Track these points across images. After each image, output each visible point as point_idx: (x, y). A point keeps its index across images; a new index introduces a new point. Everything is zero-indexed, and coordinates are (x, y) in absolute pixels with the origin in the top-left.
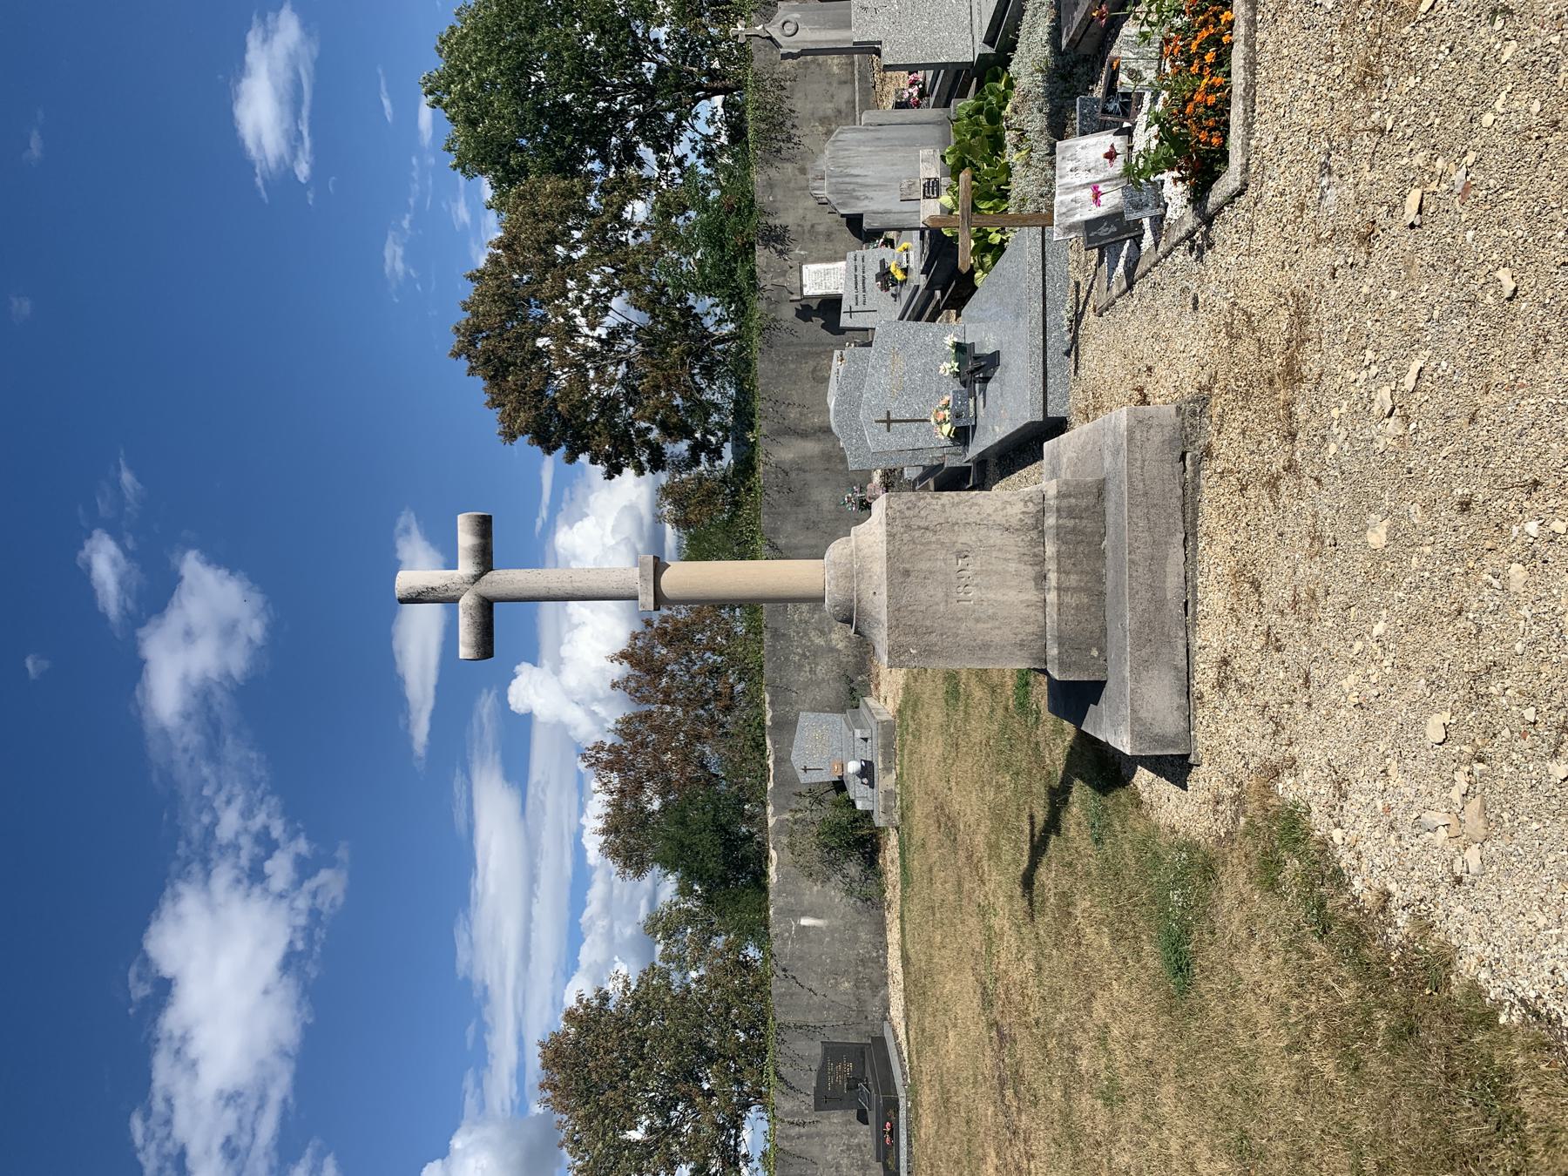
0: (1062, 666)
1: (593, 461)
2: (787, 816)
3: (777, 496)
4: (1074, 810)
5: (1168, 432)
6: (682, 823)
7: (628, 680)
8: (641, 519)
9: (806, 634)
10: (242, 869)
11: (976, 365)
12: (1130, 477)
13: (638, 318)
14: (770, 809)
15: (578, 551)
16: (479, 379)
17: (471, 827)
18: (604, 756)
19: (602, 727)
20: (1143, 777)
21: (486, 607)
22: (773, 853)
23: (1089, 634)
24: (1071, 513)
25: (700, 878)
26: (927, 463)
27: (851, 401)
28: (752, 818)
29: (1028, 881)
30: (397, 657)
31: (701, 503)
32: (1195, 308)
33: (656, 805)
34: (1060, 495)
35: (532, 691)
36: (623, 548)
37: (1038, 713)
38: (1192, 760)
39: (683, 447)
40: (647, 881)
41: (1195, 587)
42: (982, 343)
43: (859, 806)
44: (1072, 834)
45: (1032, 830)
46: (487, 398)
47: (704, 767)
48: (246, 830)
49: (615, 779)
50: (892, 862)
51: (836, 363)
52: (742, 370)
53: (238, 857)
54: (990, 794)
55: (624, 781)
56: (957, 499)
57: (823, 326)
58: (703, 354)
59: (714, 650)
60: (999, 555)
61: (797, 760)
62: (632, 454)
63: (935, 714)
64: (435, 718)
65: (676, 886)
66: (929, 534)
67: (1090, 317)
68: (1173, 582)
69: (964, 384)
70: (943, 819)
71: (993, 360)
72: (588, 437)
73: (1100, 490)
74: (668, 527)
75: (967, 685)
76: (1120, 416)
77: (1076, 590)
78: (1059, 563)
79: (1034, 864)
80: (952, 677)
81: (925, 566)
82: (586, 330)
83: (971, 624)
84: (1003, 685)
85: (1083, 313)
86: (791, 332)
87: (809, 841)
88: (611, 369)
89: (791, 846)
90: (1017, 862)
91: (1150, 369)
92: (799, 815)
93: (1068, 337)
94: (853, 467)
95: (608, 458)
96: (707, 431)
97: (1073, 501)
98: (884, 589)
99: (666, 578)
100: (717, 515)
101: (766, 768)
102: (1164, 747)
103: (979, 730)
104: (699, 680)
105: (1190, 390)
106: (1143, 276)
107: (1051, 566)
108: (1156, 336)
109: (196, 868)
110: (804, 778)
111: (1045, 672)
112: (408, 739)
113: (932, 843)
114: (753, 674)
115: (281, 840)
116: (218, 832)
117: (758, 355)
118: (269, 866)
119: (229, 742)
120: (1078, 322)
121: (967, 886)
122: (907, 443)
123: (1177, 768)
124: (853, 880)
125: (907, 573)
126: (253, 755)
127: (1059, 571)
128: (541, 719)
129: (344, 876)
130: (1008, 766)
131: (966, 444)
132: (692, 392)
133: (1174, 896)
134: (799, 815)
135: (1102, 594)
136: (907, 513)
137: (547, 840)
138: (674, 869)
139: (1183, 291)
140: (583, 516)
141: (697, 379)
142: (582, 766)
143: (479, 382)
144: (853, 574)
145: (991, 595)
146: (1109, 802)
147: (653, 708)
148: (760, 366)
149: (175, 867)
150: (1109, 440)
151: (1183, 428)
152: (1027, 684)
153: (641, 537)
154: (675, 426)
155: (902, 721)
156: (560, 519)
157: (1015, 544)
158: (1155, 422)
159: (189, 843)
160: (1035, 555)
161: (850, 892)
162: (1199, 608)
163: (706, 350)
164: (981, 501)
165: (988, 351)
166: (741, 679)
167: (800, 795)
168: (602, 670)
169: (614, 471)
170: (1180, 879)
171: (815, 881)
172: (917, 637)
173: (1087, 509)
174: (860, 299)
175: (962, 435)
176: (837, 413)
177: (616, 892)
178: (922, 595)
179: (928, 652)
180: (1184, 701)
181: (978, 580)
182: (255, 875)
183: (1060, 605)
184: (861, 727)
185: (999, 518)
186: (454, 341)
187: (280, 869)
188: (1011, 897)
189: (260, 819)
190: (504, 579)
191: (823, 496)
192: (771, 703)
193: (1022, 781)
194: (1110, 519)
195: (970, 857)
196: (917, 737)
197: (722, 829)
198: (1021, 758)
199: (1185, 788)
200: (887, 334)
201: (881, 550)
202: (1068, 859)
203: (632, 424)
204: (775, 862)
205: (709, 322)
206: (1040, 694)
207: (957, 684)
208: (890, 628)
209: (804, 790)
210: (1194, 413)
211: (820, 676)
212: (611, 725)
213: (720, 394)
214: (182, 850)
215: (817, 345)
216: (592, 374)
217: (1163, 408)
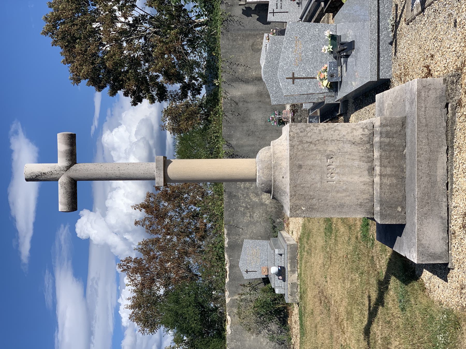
0: (382, 216)
1: (126, 94)
2: (237, 297)
3: (231, 117)
4: (391, 293)
5: (439, 93)
6: (177, 302)
7: (145, 220)
9: (248, 195)
11: (342, 48)
12: (418, 116)
13: (151, 11)
14: (227, 293)
15: (116, 145)
17: (55, 303)
18: (132, 265)
19: (130, 247)
20: (426, 275)
21: (73, 183)
22: (228, 318)
23: (396, 198)
24: (388, 135)
25: (187, 333)
26: (315, 101)
27: (273, 65)
28: (216, 299)
29: (367, 331)
30: (11, 205)
31: (187, 119)
32: (455, 26)
33: (162, 291)
34: (382, 125)
35: (89, 226)
36: (141, 144)
37: (373, 240)
38: (449, 266)
39: (178, 86)
40: (156, 336)
41: (452, 175)
42: (345, 35)
43: (277, 291)
44: (390, 306)
45: (370, 304)
46: (63, 58)
47: (190, 271)
50: (295, 322)
51: (265, 41)
52: (212, 45)
54: (348, 285)
56: (327, 127)
57: (258, 19)
58: (189, 33)
59: (195, 204)
60: (349, 157)
61: (242, 266)
62: (148, 91)
63: (319, 240)
64: (34, 241)
65: (173, 338)
66: (312, 146)
67: (403, 24)
68: (441, 172)
69: (335, 58)
70: (323, 299)
71: (351, 46)
72: (122, 80)
73: (403, 123)
74: (168, 133)
75: (336, 225)
76: (414, 84)
77: (390, 176)
78: (381, 162)
79: (370, 323)
80: (328, 221)
81: (310, 162)
82: (123, 19)
83: (334, 194)
84: (355, 225)
85: (399, 22)
86: (240, 23)
87: (249, 311)
89: (239, 314)
90: (361, 321)
91: (432, 56)
92: (243, 297)
93: (392, 34)
94: (274, 103)
95: (134, 93)
96: (192, 78)
97: (389, 128)
98: (288, 175)
100: (197, 128)
101: (224, 271)
102: (435, 259)
103: (343, 249)
104: (186, 221)
105: (451, 69)
106: (430, 5)
107: (377, 163)
108: (435, 38)
110: (246, 276)
111: (373, 219)
112: (17, 252)
113: (317, 312)
114: (217, 218)
117: (221, 36)
120: (397, 27)
121: (335, 335)
122: (304, 90)
123: (442, 270)
124: (274, 333)
125: (300, 167)
127: (381, 166)
128: (95, 242)
130: (358, 269)
131: (336, 91)
132: (182, 56)
133: (440, 338)
134: (243, 297)
135: (403, 178)
136: (301, 134)
137: (99, 310)
138: (172, 328)
139: (449, 15)
140: (118, 125)
141: (186, 47)
142: (119, 270)
143: (58, 49)
144: (271, 167)
145: (345, 178)
146: (408, 288)
147: (160, 237)
148: (222, 42)
150: (408, 96)
151: (447, 90)
152: (368, 224)
153: (152, 137)
155: (302, 244)
156: (105, 126)
157: (357, 151)
158: (432, 87)
160: (368, 157)
161: (272, 339)
162: (454, 186)
163: (191, 30)
164: (340, 128)
165: (349, 40)
166: (210, 221)
167: (244, 286)
168: (130, 215)
169: (137, 100)
170: (443, 328)
171: (252, 333)
172: (306, 202)
173: (396, 133)
174: (279, 5)
175: (334, 86)
176: (265, 73)
177: (138, 341)
178: (308, 178)
179: (311, 208)
180: (446, 235)
181: (338, 170)
183: (381, 184)
184: (279, 248)
185: (349, 137)
186: (44, 25)
188: (358, 340)
190: (82, 169)
191: (258, 117)
192: (228, 234)
193: (365, 277)
194: (408, 138)
195: (337, 319)
196: (309, 253)
197: (200, 305)
198: (364, 265)
199: (446, 281)
200: (293, 29)
201: (287, 154)
202: (388, 319)
203: (148, 73)
204: (229, 323)
205: (193, 15)
206: (373, 230)
207: (331, 224)
208: (291, 196)
209: (246, 283)
210: (453, 83)
211: (256, 219)
212: (135, 246)
213: (198, 56)
215: (254, 30)
216: (125, 44)
217: (437, 80)
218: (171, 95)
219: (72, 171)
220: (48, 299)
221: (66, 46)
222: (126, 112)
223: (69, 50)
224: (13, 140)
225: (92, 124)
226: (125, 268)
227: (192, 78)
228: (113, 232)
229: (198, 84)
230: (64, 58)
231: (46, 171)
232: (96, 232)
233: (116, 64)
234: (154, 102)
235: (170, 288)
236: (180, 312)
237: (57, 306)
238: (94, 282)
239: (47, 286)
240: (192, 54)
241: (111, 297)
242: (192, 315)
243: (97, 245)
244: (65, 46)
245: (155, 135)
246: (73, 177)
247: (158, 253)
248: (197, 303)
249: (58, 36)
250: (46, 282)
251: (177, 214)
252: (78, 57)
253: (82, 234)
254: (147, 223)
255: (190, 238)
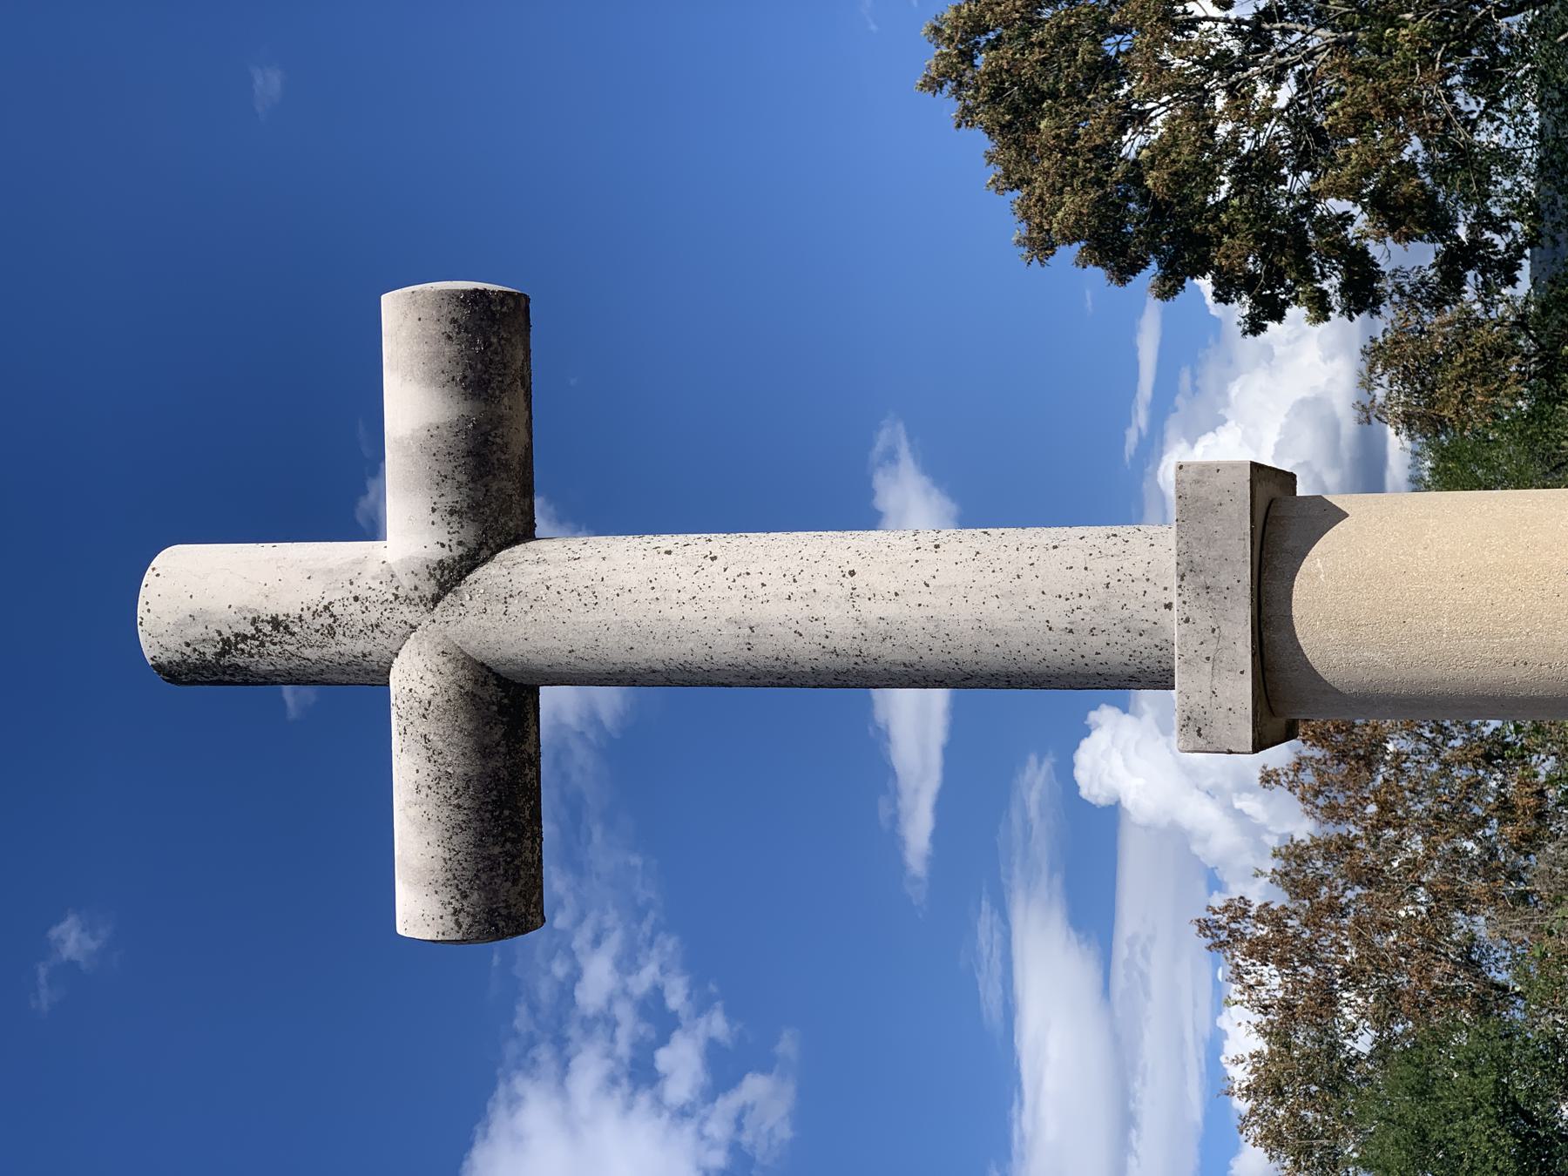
1: (1222, 297)
6: (1422, 1092)
8: (1336, 427)
10: (619, 1060)
16: (979, 134)
17: (1010, 1011)
21: (500, 703)
33: (1363, 1043)
35: (1117, 760)
48: (625, 993)
49: (1272, 979)
53: (612, 1040)
55: (1298, 985)
62: (1307, 275)
88: (1262, 90)
96: (1485, 220)
99: (1323, 584)
104: (1462, 774)
109: (544, 1053)
112: (893, 842)
115: (683, 1015)
116: (579, 994)
118: (663, 1058)
119: (597, 832)
126: (636, 860)
129: (789, 1089)
137: (1153, 1047)
140: (1217, 422)
143: (979, 141)
149: (512, 1049)
153: (1335, 459)
154: (1409, 204)
156: (1172, 429)
159: (534, 1009)
169: (1268, 311)
182: (640, 1074)
186: (930, 57)
187: (681, 1063)
189: (648, 974)
197: (1512, 1111)
214: (522, 1022)
216: (1220, 103)
218: (1400, 289)
219: (478, 603)
220: (991, 995)
221: (1006, 128)
222: (1241, 380)
223: (1016, 141)
224: (880, 480)
225: (1130, 424)
226: (1224, 936)
227: (1485, 220)
228: (1197, 787)
229: (1508, 246)
230: (1000, 170)
231: (287, 603)
232: (1141, 781)
233: (1180, 178)
234: (1327, 319)
235: (1399, 1029)
236: (1435, 1135)
237: (1017, 1020)
238: (1138, 949)
239: (986, 951)
240: (1484, 123)
241: (1195, 1005)
242: (1483, 1150)
243: (1147, 828)
244: (1002, 127)
245: (1346, 455)
246: (488, 656)
247: (1350, 894)
248: (1504, 1106)
249: (977, 90)
250: (983, 938)
251: (1424, 747)
252: (1046, 164)
253: (1095, 790)
254: (1308, 777)
255: (1478, 841)
